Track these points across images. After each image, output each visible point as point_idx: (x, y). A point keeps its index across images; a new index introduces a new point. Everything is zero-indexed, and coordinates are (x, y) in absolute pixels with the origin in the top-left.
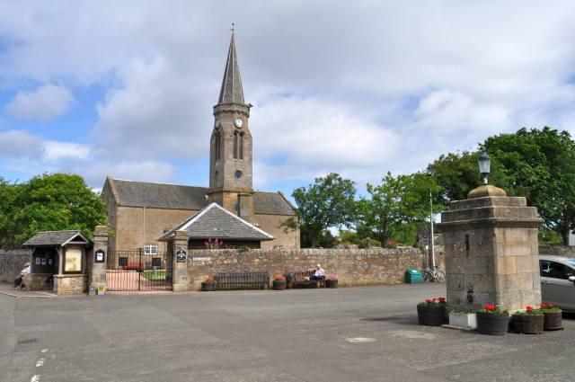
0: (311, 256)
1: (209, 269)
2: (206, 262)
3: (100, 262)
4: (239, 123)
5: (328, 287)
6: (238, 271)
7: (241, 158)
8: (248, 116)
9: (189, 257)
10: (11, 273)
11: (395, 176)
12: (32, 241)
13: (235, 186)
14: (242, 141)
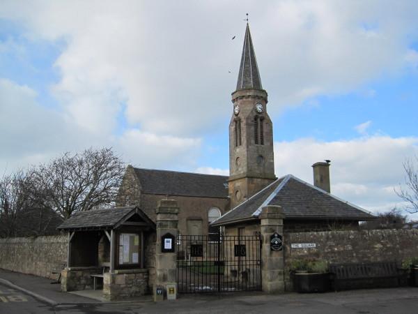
2: (309, 249)
3: (168, 251)
4: (259, 107)
6: (355, 261)
7: (262, 143)
8: (267, 102)
9: (285, 242)
13: (258, 172)
14: (262, 127)
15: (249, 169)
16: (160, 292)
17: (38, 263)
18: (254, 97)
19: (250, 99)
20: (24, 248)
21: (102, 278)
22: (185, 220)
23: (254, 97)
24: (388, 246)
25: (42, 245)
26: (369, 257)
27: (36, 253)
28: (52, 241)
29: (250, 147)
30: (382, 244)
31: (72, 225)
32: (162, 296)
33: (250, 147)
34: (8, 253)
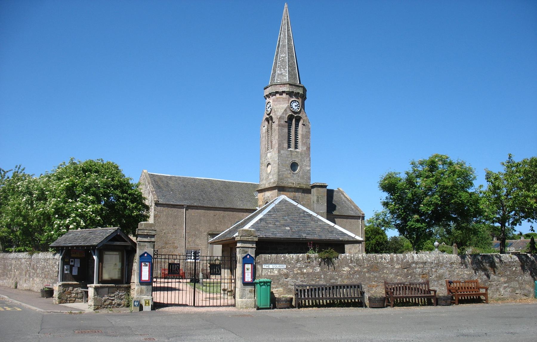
0: (417, 263)
1: (283, 280)
5: (430, 304)
6: (321, 283)
7: (296, 147)
10: (37, 280)
11: (518, 159)
12: (61, 241)
15: (280, 176)
16: (136, 304)
17: (35, 279)
18: (290, 94)
19: (284, 95)
20: (22, 264)
21: (88, 292)
22: (206, 233)
23: (290, 94)
24: (356, 269)
25: (38, 260)
26: (337, 279)
27: (33, 269)
28: (48, 257)
29: (282, 152)
30: (349, 267)
31: (62, 244)
32: (138, 308)
33: (282, 152)
34: (5, 268)
